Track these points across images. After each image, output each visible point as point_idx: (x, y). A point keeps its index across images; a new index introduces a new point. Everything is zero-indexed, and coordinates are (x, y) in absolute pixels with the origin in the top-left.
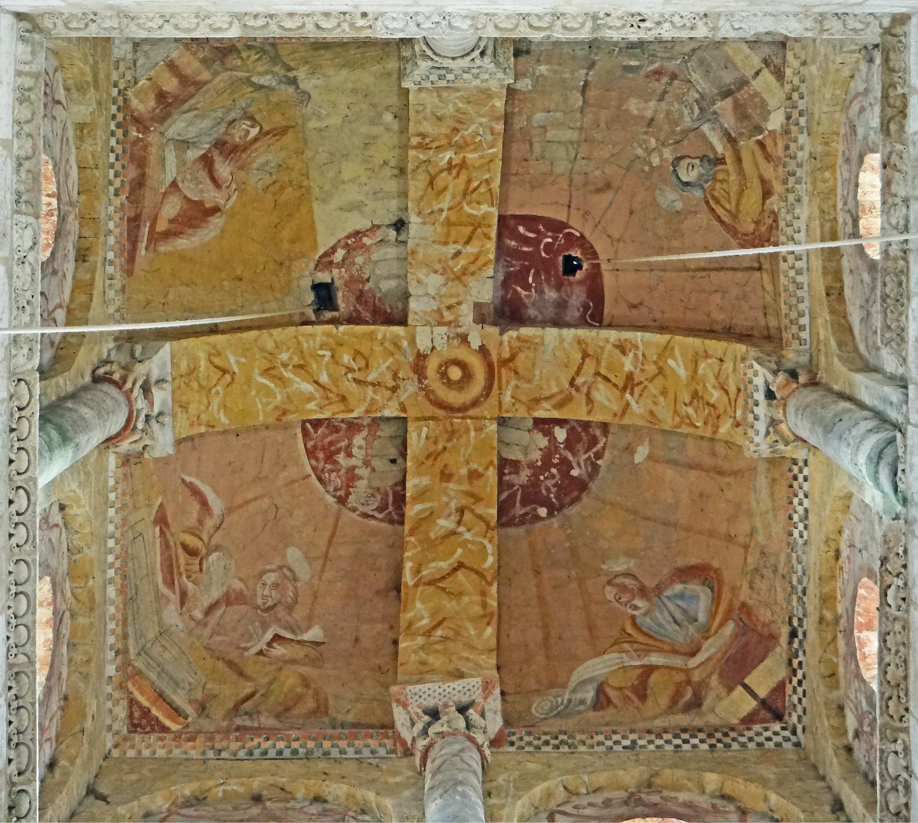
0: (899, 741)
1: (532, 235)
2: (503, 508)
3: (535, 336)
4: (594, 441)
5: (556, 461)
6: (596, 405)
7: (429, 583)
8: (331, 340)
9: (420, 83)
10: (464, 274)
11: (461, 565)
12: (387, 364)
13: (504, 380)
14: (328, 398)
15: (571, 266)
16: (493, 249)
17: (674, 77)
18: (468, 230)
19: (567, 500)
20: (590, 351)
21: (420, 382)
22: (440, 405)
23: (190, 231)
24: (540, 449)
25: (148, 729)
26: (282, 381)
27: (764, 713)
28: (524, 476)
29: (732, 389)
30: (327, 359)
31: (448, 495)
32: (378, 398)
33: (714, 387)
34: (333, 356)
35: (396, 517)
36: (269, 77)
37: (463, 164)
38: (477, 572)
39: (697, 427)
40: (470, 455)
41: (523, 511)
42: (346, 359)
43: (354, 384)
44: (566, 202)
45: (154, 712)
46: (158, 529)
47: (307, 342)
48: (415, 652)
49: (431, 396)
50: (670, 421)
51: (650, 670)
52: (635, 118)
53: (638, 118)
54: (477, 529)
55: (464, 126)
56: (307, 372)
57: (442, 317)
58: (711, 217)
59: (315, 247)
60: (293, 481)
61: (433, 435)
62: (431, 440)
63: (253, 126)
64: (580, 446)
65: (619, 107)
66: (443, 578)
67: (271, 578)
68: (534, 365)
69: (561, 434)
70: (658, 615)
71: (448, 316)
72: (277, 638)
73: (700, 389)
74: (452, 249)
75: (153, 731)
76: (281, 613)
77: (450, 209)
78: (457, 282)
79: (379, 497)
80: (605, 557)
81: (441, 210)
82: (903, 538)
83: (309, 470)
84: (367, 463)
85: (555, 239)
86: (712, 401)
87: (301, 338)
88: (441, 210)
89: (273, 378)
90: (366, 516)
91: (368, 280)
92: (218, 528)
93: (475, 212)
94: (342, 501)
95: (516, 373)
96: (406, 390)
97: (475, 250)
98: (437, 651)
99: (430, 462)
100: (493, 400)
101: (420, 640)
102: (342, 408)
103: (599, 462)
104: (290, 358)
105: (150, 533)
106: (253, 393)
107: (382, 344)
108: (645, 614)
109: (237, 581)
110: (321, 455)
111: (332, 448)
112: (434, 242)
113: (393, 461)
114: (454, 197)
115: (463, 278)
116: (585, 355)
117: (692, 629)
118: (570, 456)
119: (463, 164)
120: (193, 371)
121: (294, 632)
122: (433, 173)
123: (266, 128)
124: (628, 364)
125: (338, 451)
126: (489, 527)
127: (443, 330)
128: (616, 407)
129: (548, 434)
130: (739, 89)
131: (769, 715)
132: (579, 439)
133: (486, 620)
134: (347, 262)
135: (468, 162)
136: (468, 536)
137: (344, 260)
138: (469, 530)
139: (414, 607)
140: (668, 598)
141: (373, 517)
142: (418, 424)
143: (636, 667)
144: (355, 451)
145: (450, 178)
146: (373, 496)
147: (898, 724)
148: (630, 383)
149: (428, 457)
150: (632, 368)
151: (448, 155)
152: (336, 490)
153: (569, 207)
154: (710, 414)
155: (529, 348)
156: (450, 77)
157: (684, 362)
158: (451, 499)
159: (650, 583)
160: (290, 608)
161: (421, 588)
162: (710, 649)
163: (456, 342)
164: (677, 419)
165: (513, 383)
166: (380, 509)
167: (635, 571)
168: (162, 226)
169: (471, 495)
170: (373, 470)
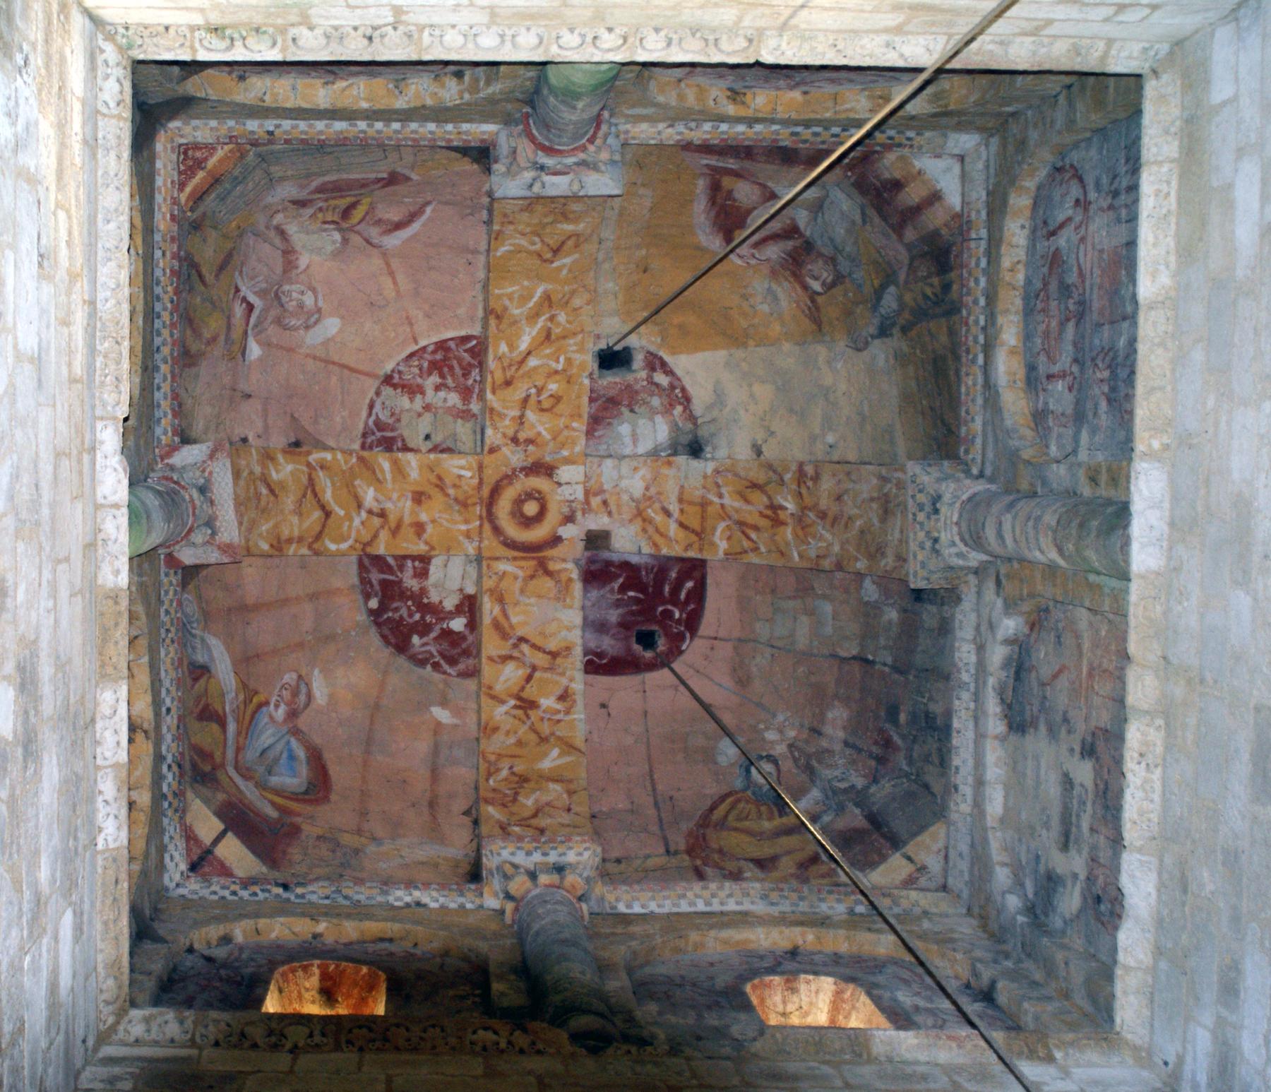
0: (325, 1040)
1: (683, 596)
2: (379, 561)
3: (573, 598)
4: (452, 661)
5: (428, 619)
6: (500, 666)
7: (311, 479)
8: (575, 371)
9: (913, 482)
10: (644, 520)
11: (328, 514)
12: (544, 433)
13: (523, 563)
14: (510, 365)
15: (647, 640)
16: (673, 554)
17: (881, 760)
18: (695, 524)
19: (386, 631)
20: (559, 661)
21: (522, 469)
22: (496, 491)
23: (713, 214)
24: (441, 602)
25: (182, 168)
26: (533, 317)
27: (196, 853)
28: (411, 583)
29: (542, 822)
30: (554, 365)
31: (399, 499)
32: (507, 422)
33: (537, 801)
34: (556, 372)
35: (369, 440)
36: (895, 306)
37: (777, 522)
38: (321, 532)
39: (487, 780)
40: (441, 525)
41: (375, 582)
42: (553, 387)
43: (524, 395)
44: (721, 635)
45: (201, 175)
46: (385, 175)
47: (575, 344)
48: (248, 465)
49: (505, 482)
50: (491, 749)
51: (223, 724)
52: (823, 714)
53: (822, 717)
54: (363, 532)
55: (828, 526)
56: (542, 344)
57: (596, 495)
58: (716, 798)
59: (674, 353)
60: (411, 324)
61: (463, 483)
62: (457, 481)
63: (823, 284)
64: (445, 645)
65: (836, 696)
66: (315, 495)
67: (309, 300)
68: (539, 596)
69: (458, 624)
70: (269, 732)
71: (596, 501)
72: (251, 308)
73: (532, 784)
74: (674, 508)
75: (180, 173)
76: (273, 313)
77: (722, 506)
78: (635, 512)
79: (390, 421)
80: (326, 672)
81: (721, 496)
82: (552, 1050)
83: (423, 343)
84: (427, 408)
85: (679, 621)
86: (520, 798)
87: (580, 337)
88: (721, 496)
89: (540, 305)
90: (371, 406)
91: (632, 411)
92: (368, 241)
93: (718, 533)
94: (388, 380)
95: (532, 577)
96: (513, 453)
97: (672, 534)
98: (248, 489)
99: (434, 480)
100: (502, 551)
101: (258, 470)
102: (498, 382)
103: (429, 667)
104: (559, 324)
105: (383, 168)
106: (526, 283)
107: (567, 427)
108: (271, 717)
109: (307, 261)
110: (439, 356)
111: (446, 370)
112: (682, 487)
113: (427, 437)
114: (737, 511)
115: (639, 519)
116: (554, 655)
117: (261, 769)
118: (433, 635)
119: (777, 522)
120: (565, 216)
121: (256, 326)
122: (767, 488)
123: (820, 299)
124: (548, 702)
125: (442, 376)
126: (368, 544)
127: (580, 494)
128: (499, 688)
129: (459, 610)
130: (884, 836)
131: (195, 858)
132: (454, 644)
133: (275, 543)
134: (653, 388)
135: (782, 528)
136: (357, 522)
137: (657, 385)
138: (363, 523)
139: (287, 462)
140: (288, 742)
141: (370, 415)
142: (475, 465)
143: (224, 708)
144: (442, 394)
145: (761, 508)
146: (393, 414)
147: (343, 1039)
148: (527, 705)
149: (440, 478)
150: (544, 707)
151: (790, 506)
152: (400, 372)
153: (716, 638)
154: (506, 795)
155: (560, 592)
156: (921, 517)
157: (559, 766)
158: (394, 503)
159: (303, 722)
160: (278, 321)
161: (305, 469)
162: (249, 791)
163: (566, 510)
164: (493, 758)
165: (520, 573)
166: (378, 423)
167: (313, 706)
168: (727, 182)
169: (399, 526)
170: (420, 415)
